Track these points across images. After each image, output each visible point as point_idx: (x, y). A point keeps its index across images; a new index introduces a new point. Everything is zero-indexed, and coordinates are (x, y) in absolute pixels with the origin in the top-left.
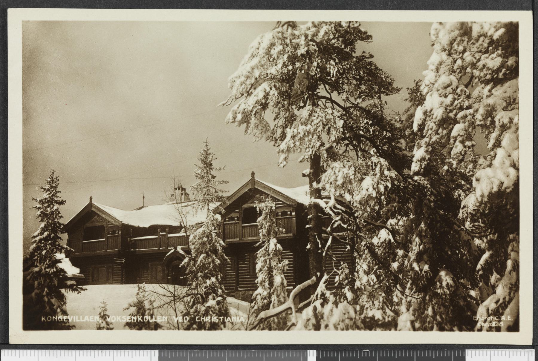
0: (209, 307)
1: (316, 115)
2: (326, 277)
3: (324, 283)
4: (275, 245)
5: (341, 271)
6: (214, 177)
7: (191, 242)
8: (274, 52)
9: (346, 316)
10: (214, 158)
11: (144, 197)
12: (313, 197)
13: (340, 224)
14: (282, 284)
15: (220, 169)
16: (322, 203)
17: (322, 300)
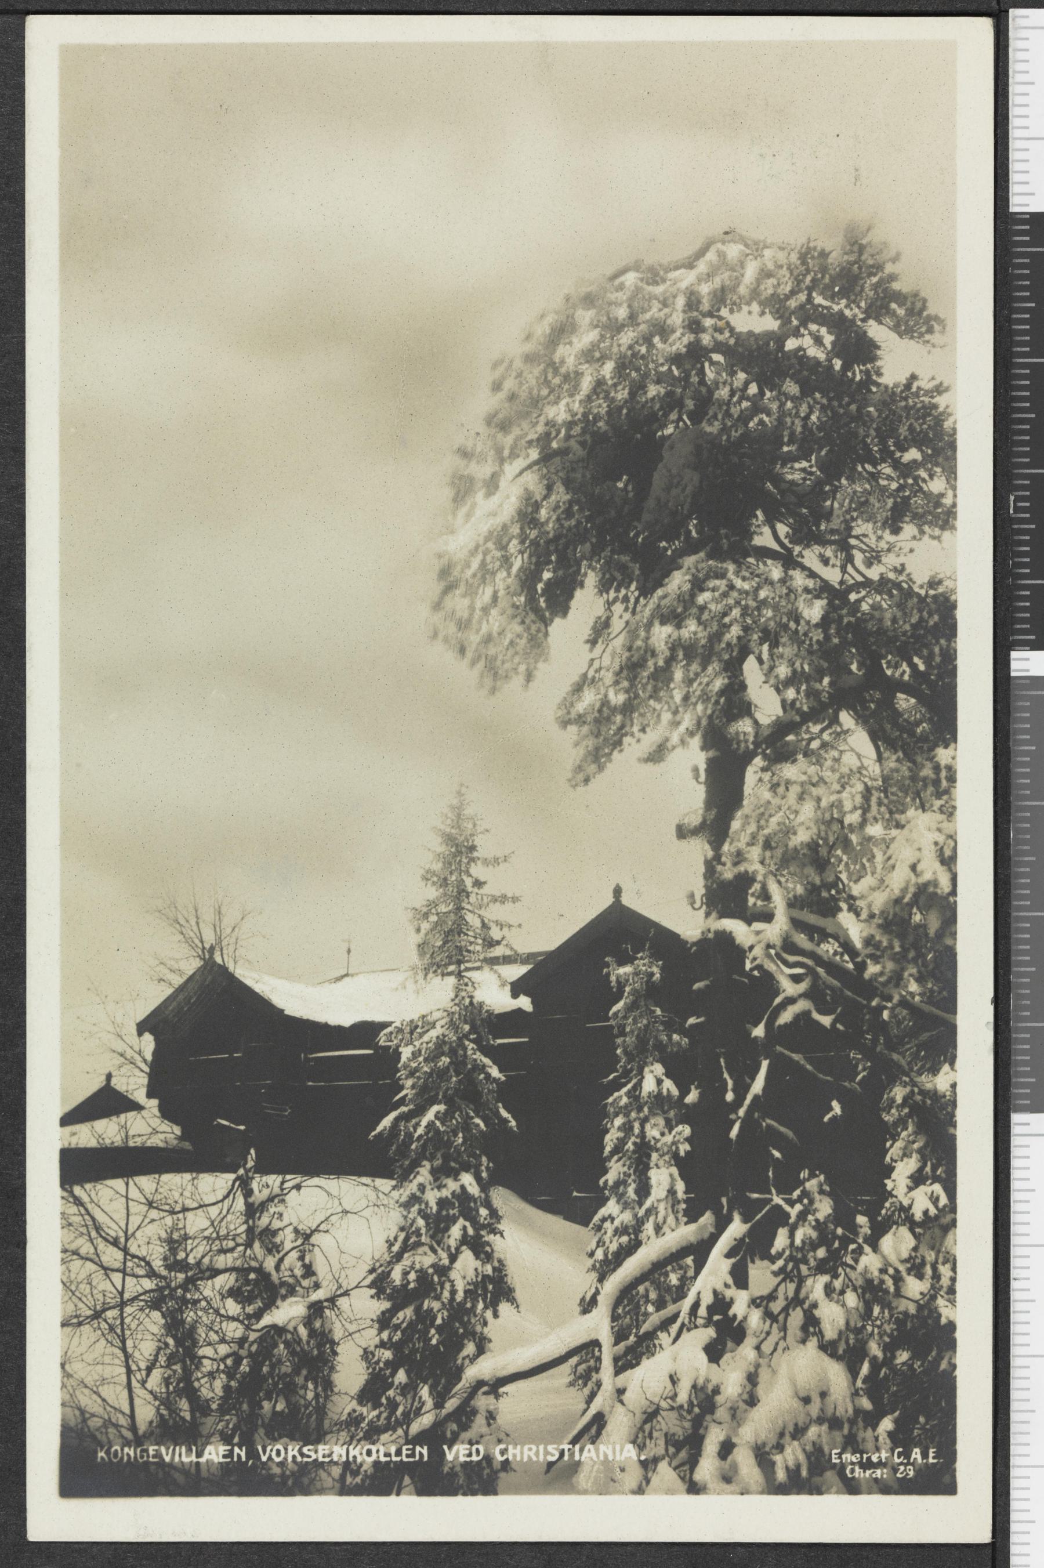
0: (274, 1327)
1: (721, 584)
2: (737, 1228)
3: (728, 1255)
4: (659, 1082)
5: (798, 1207)
6: (478, 884)
7: (405, 1067)
8: (568, 354)
9: (814, 1409)
10: (479, 829)
11: (349, 951)
12: (714, 915)
13: (805, 1015)
14: (672, 1192)
15: (496, 861)
16: (739, 930)
17: (711, 1333)
